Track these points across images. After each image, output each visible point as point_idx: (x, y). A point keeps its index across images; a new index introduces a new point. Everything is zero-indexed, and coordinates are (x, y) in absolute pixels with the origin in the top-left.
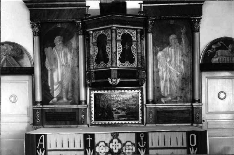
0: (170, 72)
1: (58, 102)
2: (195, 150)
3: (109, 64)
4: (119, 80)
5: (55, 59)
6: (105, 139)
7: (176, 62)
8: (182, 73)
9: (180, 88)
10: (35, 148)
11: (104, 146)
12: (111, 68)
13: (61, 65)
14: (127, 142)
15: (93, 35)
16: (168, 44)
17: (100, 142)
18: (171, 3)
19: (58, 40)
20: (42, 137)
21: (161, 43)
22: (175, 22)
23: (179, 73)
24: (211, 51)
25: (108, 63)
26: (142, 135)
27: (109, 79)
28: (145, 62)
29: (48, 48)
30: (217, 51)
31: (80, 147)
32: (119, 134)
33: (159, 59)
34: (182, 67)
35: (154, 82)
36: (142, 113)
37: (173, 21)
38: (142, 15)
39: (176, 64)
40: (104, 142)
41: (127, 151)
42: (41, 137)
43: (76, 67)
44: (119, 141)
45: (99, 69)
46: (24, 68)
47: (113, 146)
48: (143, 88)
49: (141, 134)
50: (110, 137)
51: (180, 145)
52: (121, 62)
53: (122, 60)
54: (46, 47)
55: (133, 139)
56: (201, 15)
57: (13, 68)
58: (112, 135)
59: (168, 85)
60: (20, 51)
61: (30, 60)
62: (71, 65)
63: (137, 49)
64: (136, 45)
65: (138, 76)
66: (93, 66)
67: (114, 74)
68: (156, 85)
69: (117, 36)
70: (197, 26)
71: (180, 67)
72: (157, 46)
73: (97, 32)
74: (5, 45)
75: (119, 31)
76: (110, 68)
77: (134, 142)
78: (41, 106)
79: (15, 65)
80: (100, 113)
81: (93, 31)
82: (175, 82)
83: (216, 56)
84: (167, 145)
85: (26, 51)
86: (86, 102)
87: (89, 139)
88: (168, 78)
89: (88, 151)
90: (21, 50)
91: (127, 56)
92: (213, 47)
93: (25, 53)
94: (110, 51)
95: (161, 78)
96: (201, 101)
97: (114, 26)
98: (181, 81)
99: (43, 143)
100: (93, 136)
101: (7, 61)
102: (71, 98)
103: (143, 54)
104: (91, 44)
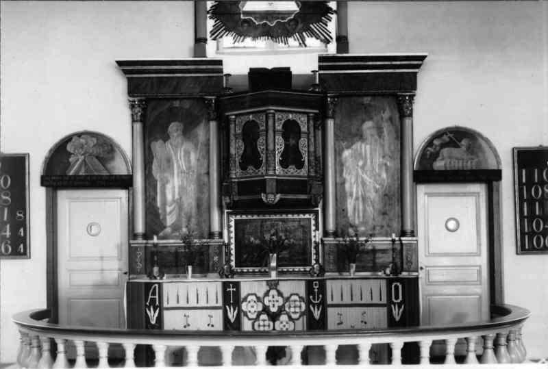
0: (364, 184)
1: (174, 234)
2: (400, 307)
3: (262, 170)
4: (278, 196)
5: (169, 161)
6: (256, 290)
7: (373, 167)
8: (383, 186)
9: (380, 211)
10: (143, 306)
11: (250, 312)
12: (266, 177)
13: (180, 170)
14: (291, 295)
15: (235, 121)
16: (360, 136)
17: (249, 295)
18: (372, 61)
19: (174, 128)
20: (155, 287)
21: (350, 136)
22: (371, 101)
23: (378, 186)
24: (432, 150)
25: (260, 169)
26: (316, 284)
27: (262, 194)
28: (321, 167)
29: (157, 141)
30: (442, 150)
31: (217, 302)
32: (280, 282)
33: (346, 161)
34: (384, 175)
35: (336, 200)
36: (317, 254)
37: (369, 98)
38: (317, 90)
39: (373, 169)
40: (255, 295)
41: (292, 310)
42: (153, 287)
43: (206, 175)
44: (280, 294)
45: (246, 178)
46: (116, 176)
47: (270, 301)
48: (318, 211)
49: (314, 283)
50: (265, 288)
51: (376, 301)
52: (282, 167)
53: (284, 164)
54: (153, 140)
55: (302, 291)
56: (415, 89)
57: (97, 176)
58: (268, 284)
59: (361, 207)
60: (110, 147)
61: (126, 162)
62: (195, 170)
63: (308, 146)
64: (306, 140)
65: (310, 191)
66: (236, 174)
67: (271, 186)
68: (339, 205)
69: (276, 125)
70: (407, 108)
71: (380, 176)
72: (342, 140)
73: (242, 118)
74: (83, 136)
75: (280, 117)
76: (263, 176)
77: (303, 293)
78: (145, 241)
79: (100, 171)
80: (245, 254)
81: (236, 115)
82: (371, 202)
83: (440, 158)
84: (357, 300)
85: (119, 147)
86: (221, 235)
87: (231, 290)
88: (360, 193)
89: (230, 309)
90: (111, 145)
91: (291, 157)
92: (436, 142)
93: (117, 150)
94: (263, 149)
95: (348, 194)
96: (415, 234)
97: (271, 108)
98: (382, 199)
99: (157, 297)
100: (237, 285)
101: (86, 164)
102: (196, 227)
103: (317, 153)
104: (232, 137)
